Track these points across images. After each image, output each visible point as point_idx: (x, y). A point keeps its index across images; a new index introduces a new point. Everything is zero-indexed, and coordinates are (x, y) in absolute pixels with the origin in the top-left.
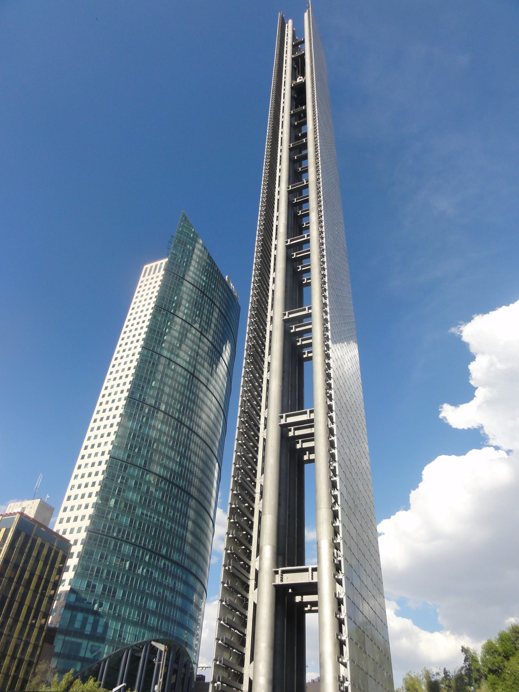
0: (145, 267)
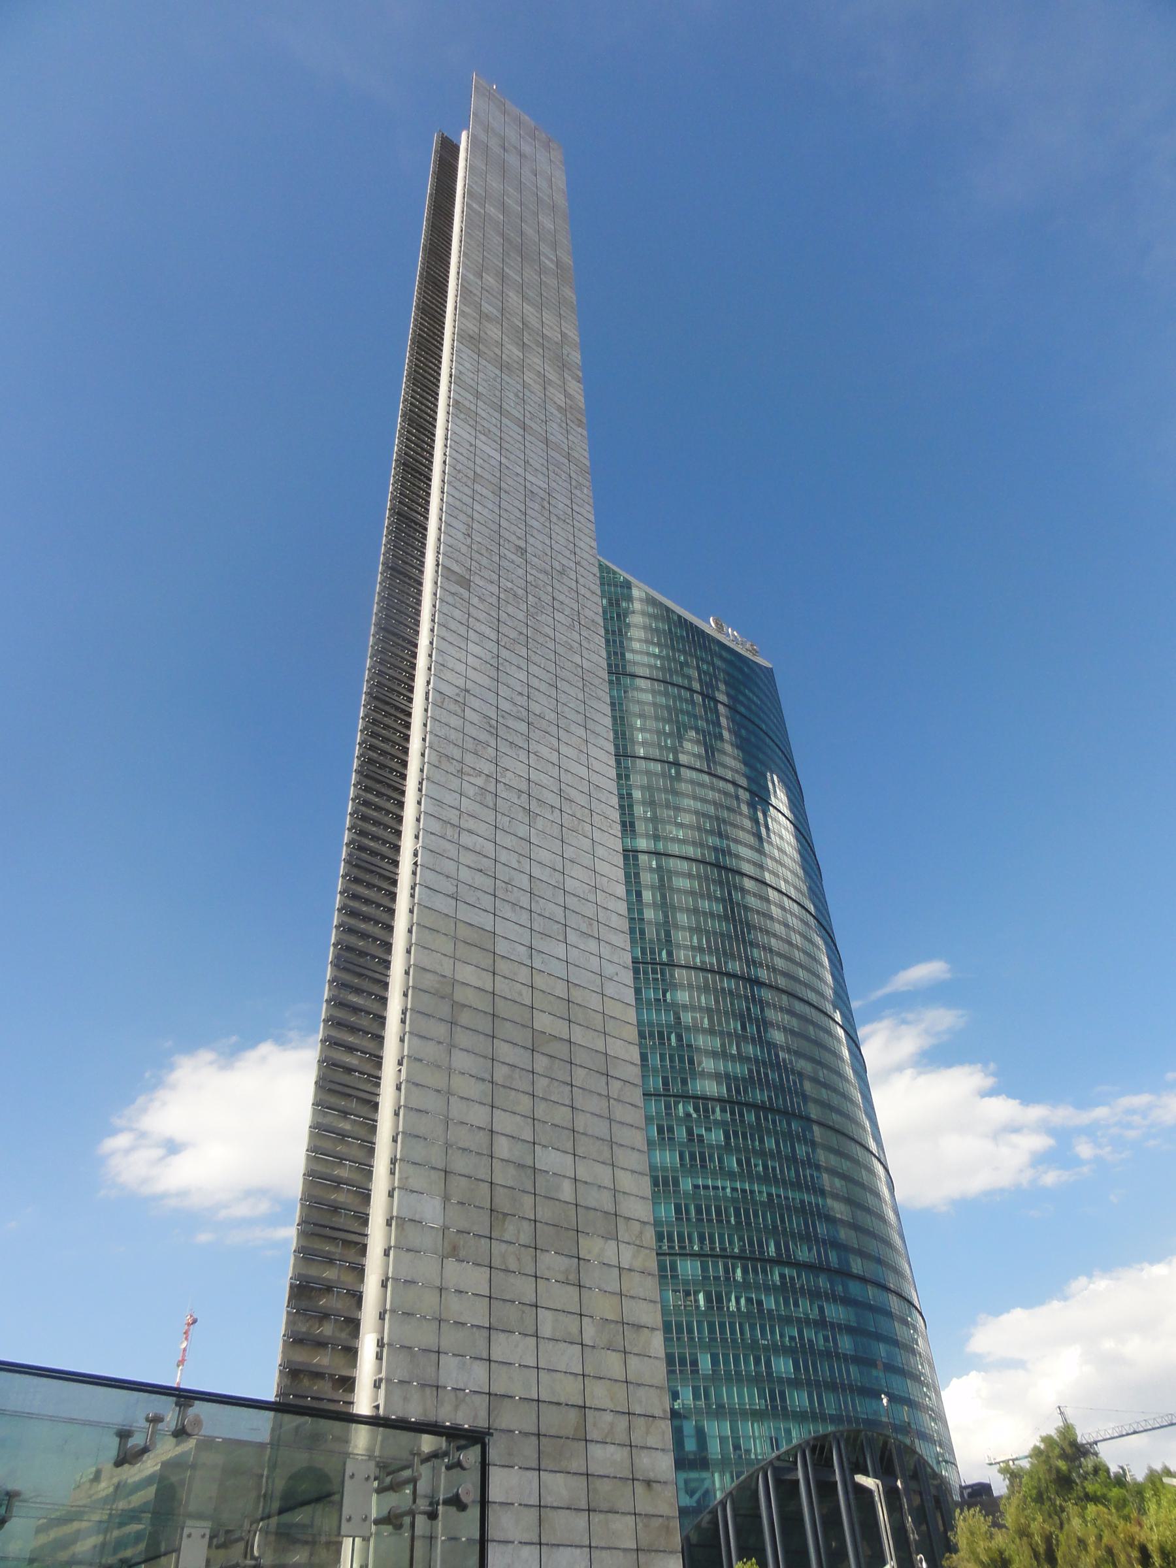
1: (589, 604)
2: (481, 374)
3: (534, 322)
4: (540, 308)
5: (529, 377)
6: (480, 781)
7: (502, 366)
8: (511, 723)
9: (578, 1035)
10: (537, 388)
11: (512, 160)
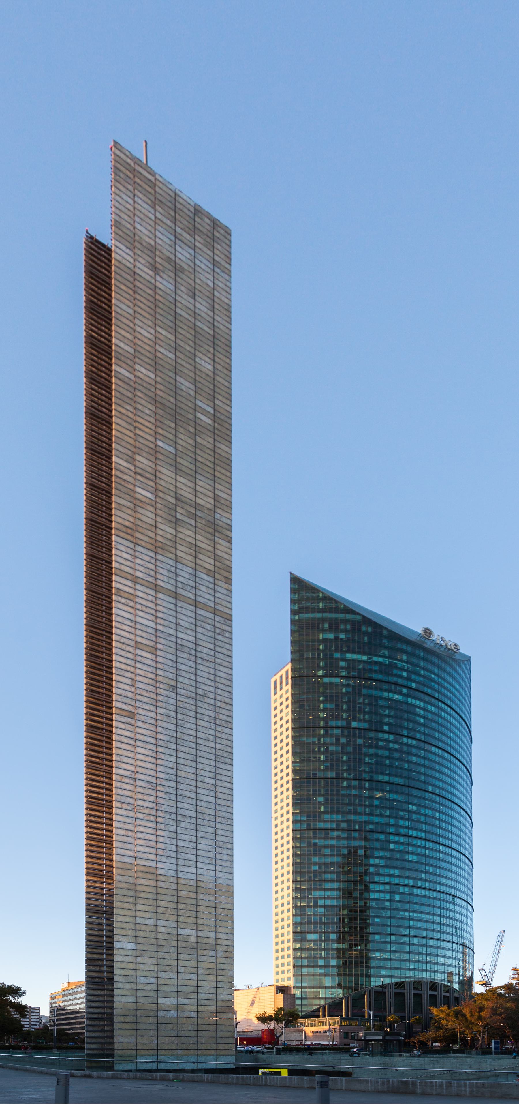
3: (186, 493)
7: (156, 548)
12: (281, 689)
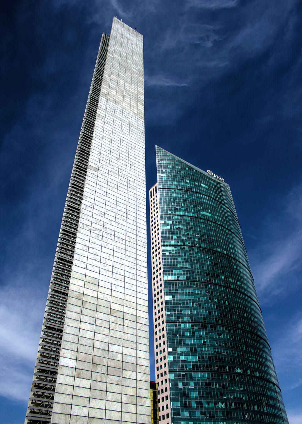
0: (150, 191)
1: (141, 174)
2: (108, 106)
3: (128, 88)
4: (130, 84)
5: (125, 105)
6: (97, 232)
7: (116, 102)
8: (109, 213)
9: (126, 310)
10: (127, 108)
11: (125, 41)
12: (154, 195)
